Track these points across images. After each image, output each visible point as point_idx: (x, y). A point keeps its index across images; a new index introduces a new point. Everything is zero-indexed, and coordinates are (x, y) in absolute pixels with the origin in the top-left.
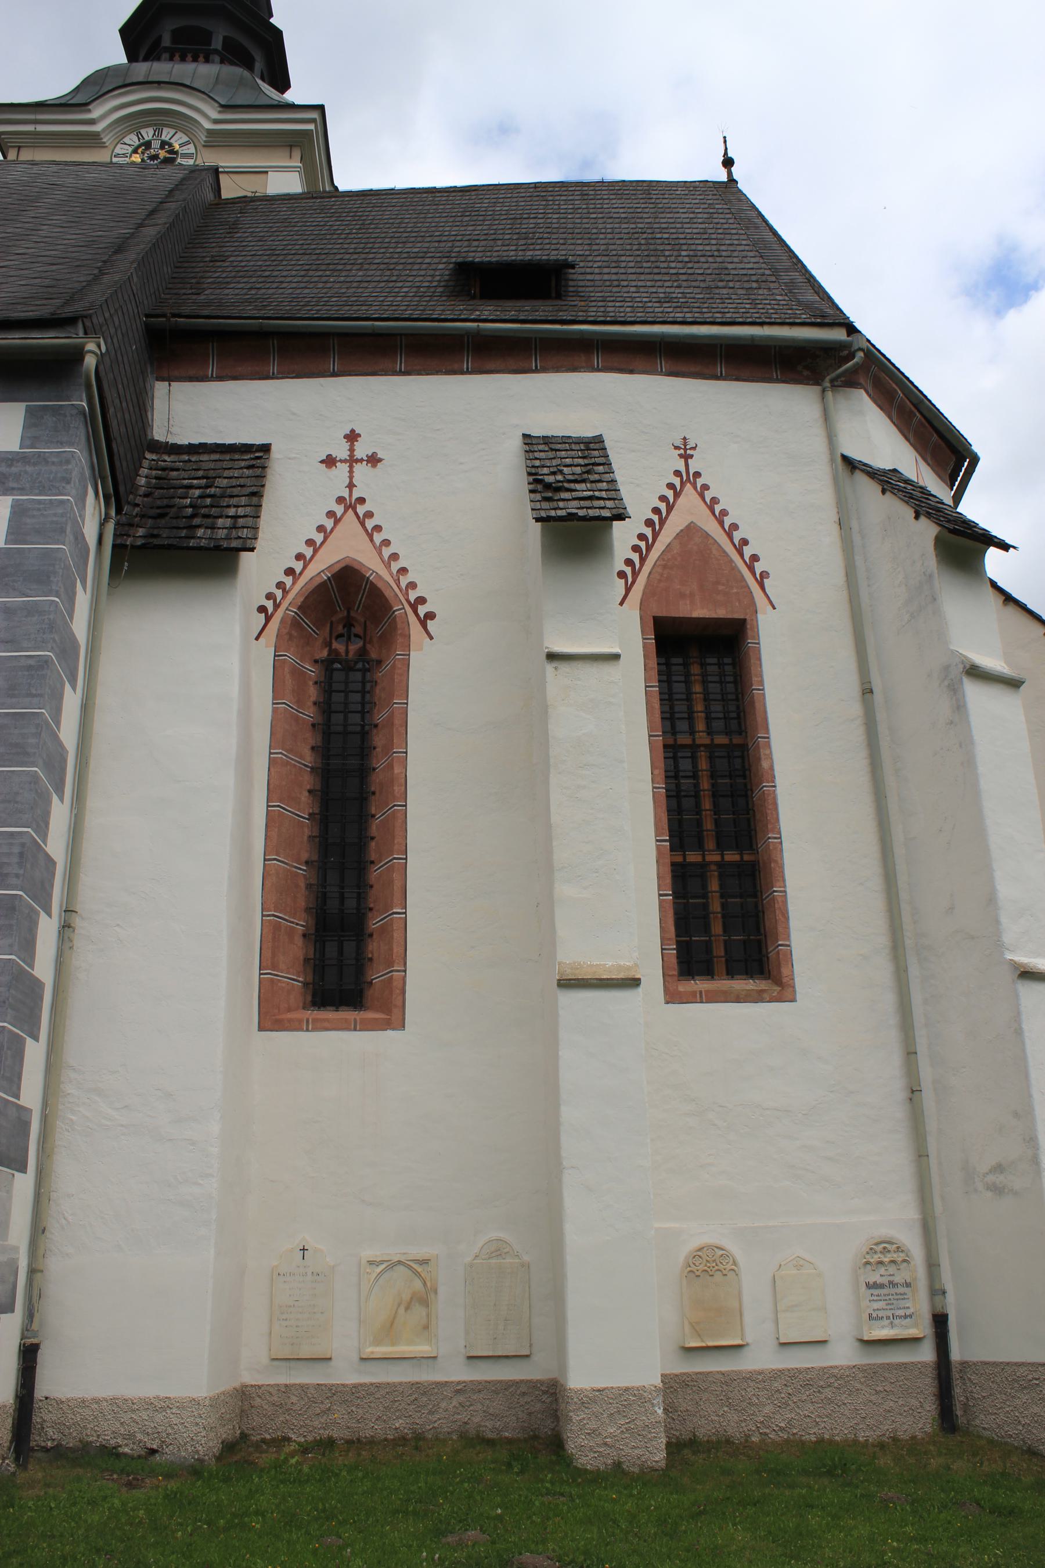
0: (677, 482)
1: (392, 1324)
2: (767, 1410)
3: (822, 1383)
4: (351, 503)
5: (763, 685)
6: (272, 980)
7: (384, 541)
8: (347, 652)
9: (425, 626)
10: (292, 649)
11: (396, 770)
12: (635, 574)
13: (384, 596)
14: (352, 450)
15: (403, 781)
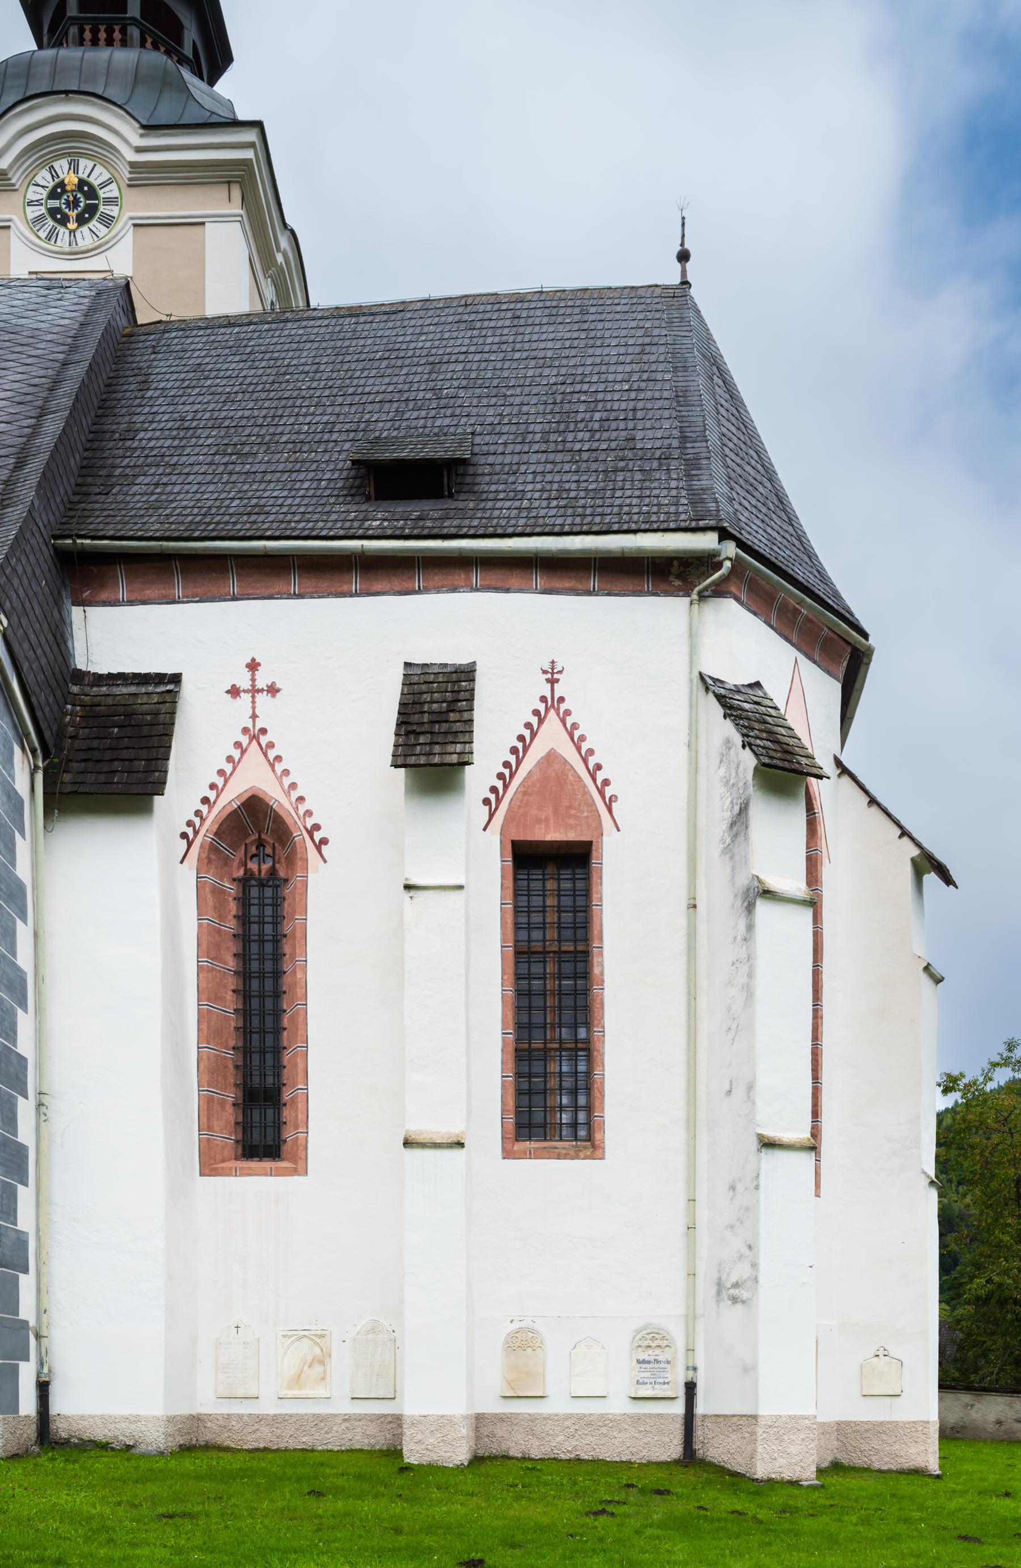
0: (542, 707)
1: (299, 1376)
2: (561, 1438)
3: (600, 1424)
4: (254, 735)
5: (601, 901)
6: (208, 1139)
7: (284, 770)
8: (260, 871)
9: (320, 851)
10: (212, 871)
11: (299, 975)
12: (499, 801)
13: (285, 823)
14: (253, 680)
15: (304, 984)
